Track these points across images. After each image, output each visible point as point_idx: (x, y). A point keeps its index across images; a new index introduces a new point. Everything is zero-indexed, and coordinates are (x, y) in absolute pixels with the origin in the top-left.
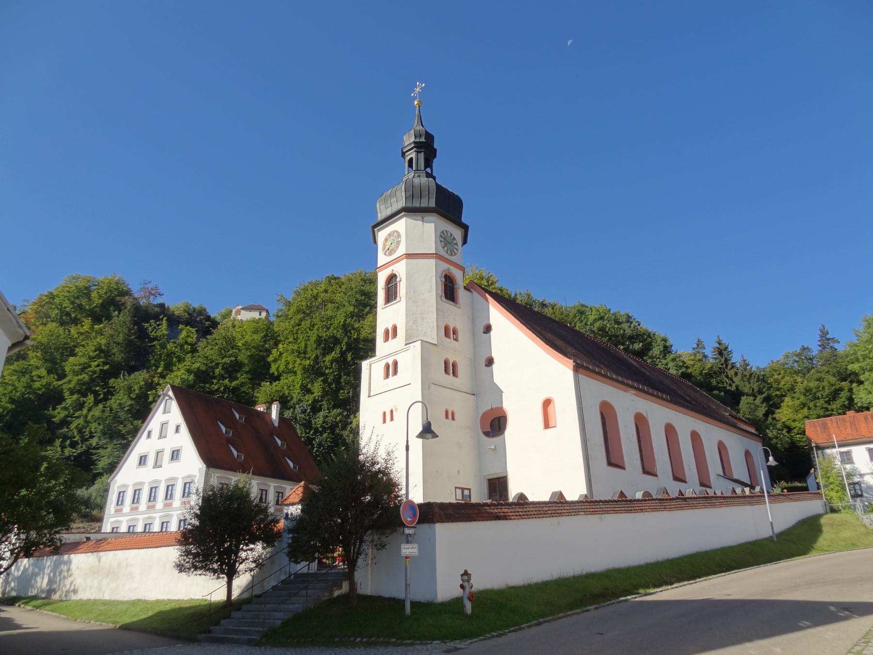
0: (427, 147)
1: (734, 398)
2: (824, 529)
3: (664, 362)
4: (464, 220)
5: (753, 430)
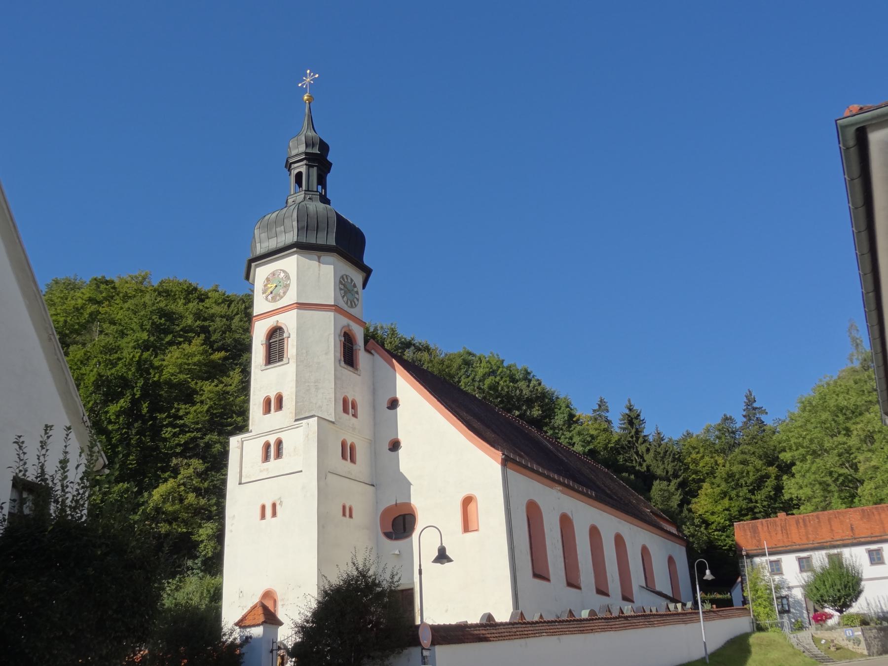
0: (319, 160)
1: (645, 480)
2: (753, 650)
3: (568, 435)
4: (367, 260)
5: (674, 530)
